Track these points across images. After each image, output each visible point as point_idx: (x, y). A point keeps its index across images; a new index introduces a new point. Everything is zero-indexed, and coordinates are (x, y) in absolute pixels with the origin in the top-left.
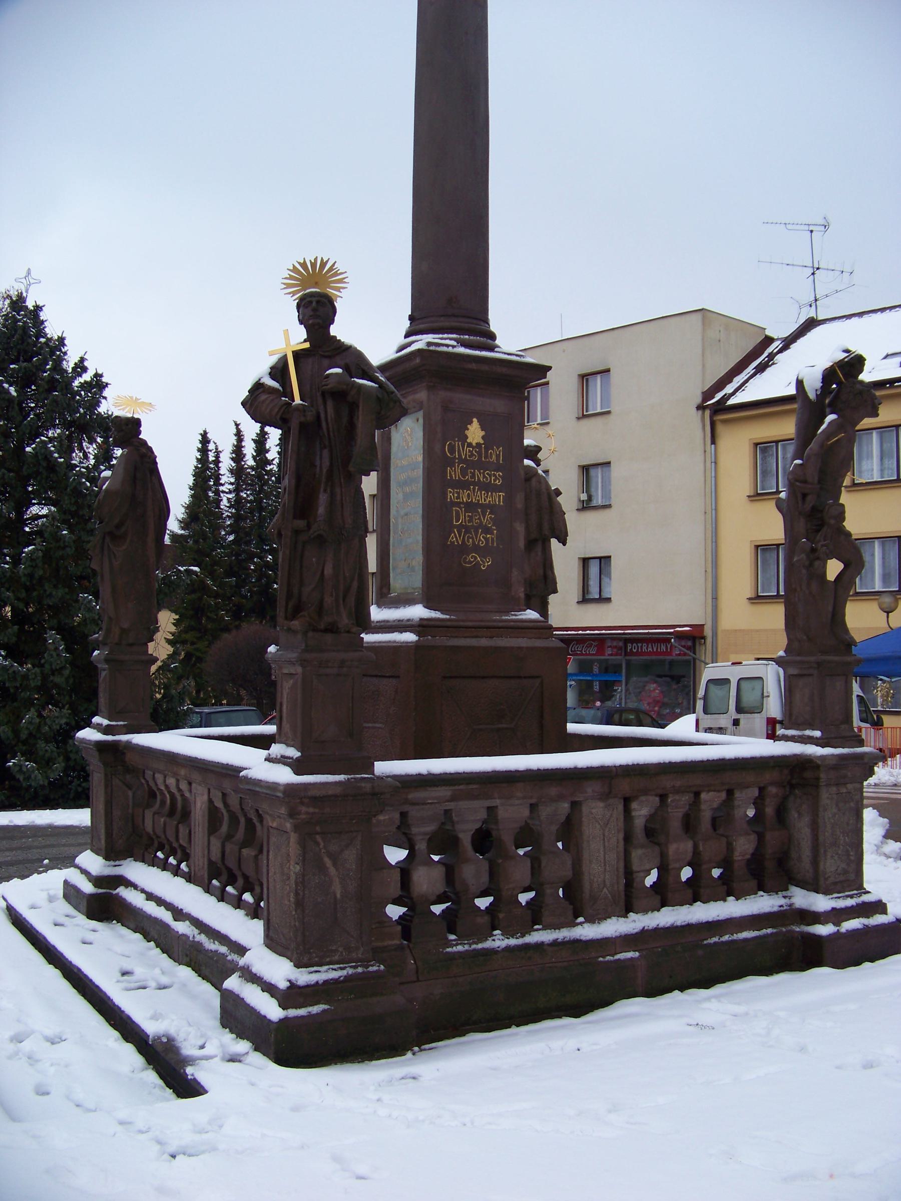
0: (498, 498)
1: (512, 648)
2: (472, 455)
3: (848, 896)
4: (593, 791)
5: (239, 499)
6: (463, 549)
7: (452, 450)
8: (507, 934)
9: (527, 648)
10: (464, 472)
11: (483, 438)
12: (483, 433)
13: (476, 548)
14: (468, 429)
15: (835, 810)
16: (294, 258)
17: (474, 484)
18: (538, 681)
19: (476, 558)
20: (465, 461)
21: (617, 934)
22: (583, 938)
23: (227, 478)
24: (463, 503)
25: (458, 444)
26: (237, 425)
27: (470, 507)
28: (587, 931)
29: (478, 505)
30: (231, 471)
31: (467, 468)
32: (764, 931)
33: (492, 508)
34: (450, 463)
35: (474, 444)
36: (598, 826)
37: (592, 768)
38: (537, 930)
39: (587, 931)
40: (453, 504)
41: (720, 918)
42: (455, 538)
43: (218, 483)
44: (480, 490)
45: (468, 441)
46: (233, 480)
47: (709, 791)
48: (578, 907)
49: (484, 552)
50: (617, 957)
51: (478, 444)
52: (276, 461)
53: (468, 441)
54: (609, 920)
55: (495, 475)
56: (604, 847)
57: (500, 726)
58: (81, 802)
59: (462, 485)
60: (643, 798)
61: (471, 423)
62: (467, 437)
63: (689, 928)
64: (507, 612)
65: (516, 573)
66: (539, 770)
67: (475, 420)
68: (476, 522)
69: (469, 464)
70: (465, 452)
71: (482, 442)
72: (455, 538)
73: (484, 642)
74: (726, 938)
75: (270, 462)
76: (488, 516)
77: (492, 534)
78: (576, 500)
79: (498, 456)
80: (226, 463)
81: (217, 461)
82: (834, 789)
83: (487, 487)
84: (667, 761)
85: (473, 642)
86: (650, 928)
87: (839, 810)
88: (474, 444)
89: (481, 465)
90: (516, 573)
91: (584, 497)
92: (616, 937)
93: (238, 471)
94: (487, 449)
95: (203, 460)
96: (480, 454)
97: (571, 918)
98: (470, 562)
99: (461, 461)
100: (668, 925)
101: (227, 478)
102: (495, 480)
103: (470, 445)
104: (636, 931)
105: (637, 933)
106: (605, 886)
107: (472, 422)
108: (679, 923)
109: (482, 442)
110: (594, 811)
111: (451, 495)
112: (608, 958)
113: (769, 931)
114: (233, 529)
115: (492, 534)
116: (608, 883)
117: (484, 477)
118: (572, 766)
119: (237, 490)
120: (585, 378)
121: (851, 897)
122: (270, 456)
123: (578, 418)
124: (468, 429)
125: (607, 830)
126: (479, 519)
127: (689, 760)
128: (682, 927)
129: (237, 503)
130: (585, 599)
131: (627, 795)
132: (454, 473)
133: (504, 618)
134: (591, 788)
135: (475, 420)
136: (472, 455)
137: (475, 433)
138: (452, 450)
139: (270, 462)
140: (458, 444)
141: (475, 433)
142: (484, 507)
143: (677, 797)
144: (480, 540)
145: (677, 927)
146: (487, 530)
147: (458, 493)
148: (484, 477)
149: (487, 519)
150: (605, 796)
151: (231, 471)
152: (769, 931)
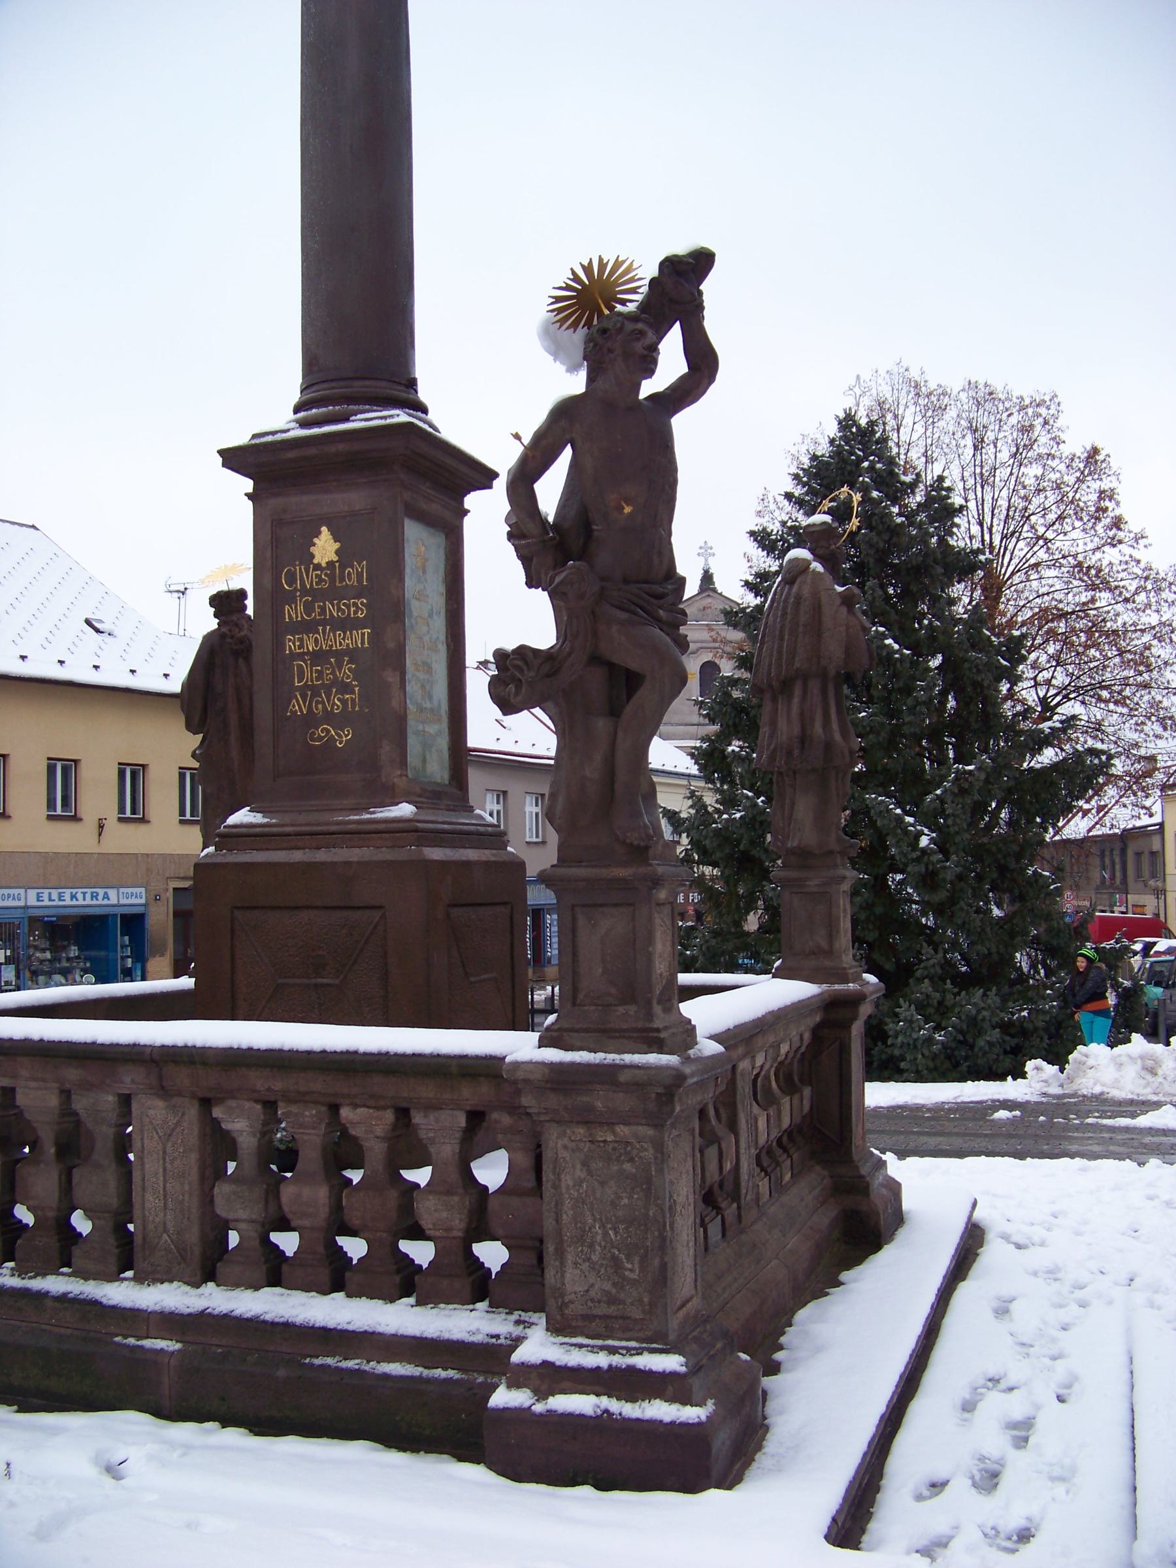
0: (359, 638)
1: (334, 864)
2: (321, 580)
3: (602, 1348)
4: (133, 1081)
6: (311, 720)
7: (291, 580)
8: (20, 1272)
9: (358, 862)
10: (309, 608)
11: (337, 552)
12: (337, 545)
13: (329, 717)
14: (314, 545)
15: (580, 1173)
17: (324, 623)
18: (377, 914)
19: (328, 731)
20: (311, 592)
21: (157, 1308)
22: (104, 1301)
24: (308, 653)
25: (299, 569)
27: (318, 657)
28: (122, 1293)
29: (330, 652)
31: (313, 602)
32: (440, 1373)
33: (352, 654)
34: (290, 599)
35: (324, 565)
36: (156, 1137)
37: (420, 1055)
38: (63, 1274)
39: (122, 1293)
40: (294, 656)
41: (350, 1328)
42: (298, 706)
44: (333, 630)
45: (315, 561)
47: (356, 1106)
48: (126, 1258)
49: (339, 721)
50: (148, 1343)
51: (330, 564)
53: (315, 561)
54: (166, 1285)
55: (355, 604)
56: (165, 1169)
57: (320, 980)
58: (886, 1074)
59: (308, 627)
60: (232, 1103)
61: (318, 534)
62: (313, 556)
63: (286, 1329)
64: (366, 809)
65: (388, 748)
66: (324, 1052)
67: (324, 529)
68: (328, 676)
70: (310, 580)
71: (335, 558)
72: (298, 706)
73: (297, 856)
74: (351, 1364)
76: (346, 669)
77: (353, 692)
79: (360, 575)
82: (581, 1131)
83: (346, 624)
84: (244, 1046)
86: (216, 1312)
87: (590, 1173)
88: (324, 565)
89: (334, 593)
90: (388, 748)
92: (155, 1312)
94: (343, 567)
97: (114, 1268)
98: (320, 738)
99: (305, 592)
100: (249, 1315)
102: (356, 612)
103: (318, 567)
104: (188, 1311)
105: (190, 1315)
106: (165, 1230)
107: (320, 533)
108: (268, 1317)
109: (335, 558)
110: (151, 1112)
111: (291, 644)
112: (132, 1341)
113: (451, 1373)
115: (353, 692)
116: (170, 1226)
117: (339, 609)
118: (89, 1040)
121: (613, 1351)
124: (314, 545)
125: (170, 1144)
126: (333, 673)
127: (180, 1043)
128: (273, 1324)
131: (209, 1095)
132: (293, 612)
133: (352, 817)
134: (129, 1078)
135: (324, 529)
136: (321, 580)
137: (325, 548)
138: (291, 580)
140: (299, 569)
141: (325, 548)
142: (339, 654)
143: (294, 1109)
144: (334, 704)
145: (265, 1322)
146: (345, 688)
147: (301, 640)
148: (339, 609)
149: (346, 672)
150: (163, 1091)
152: (451, 1373)
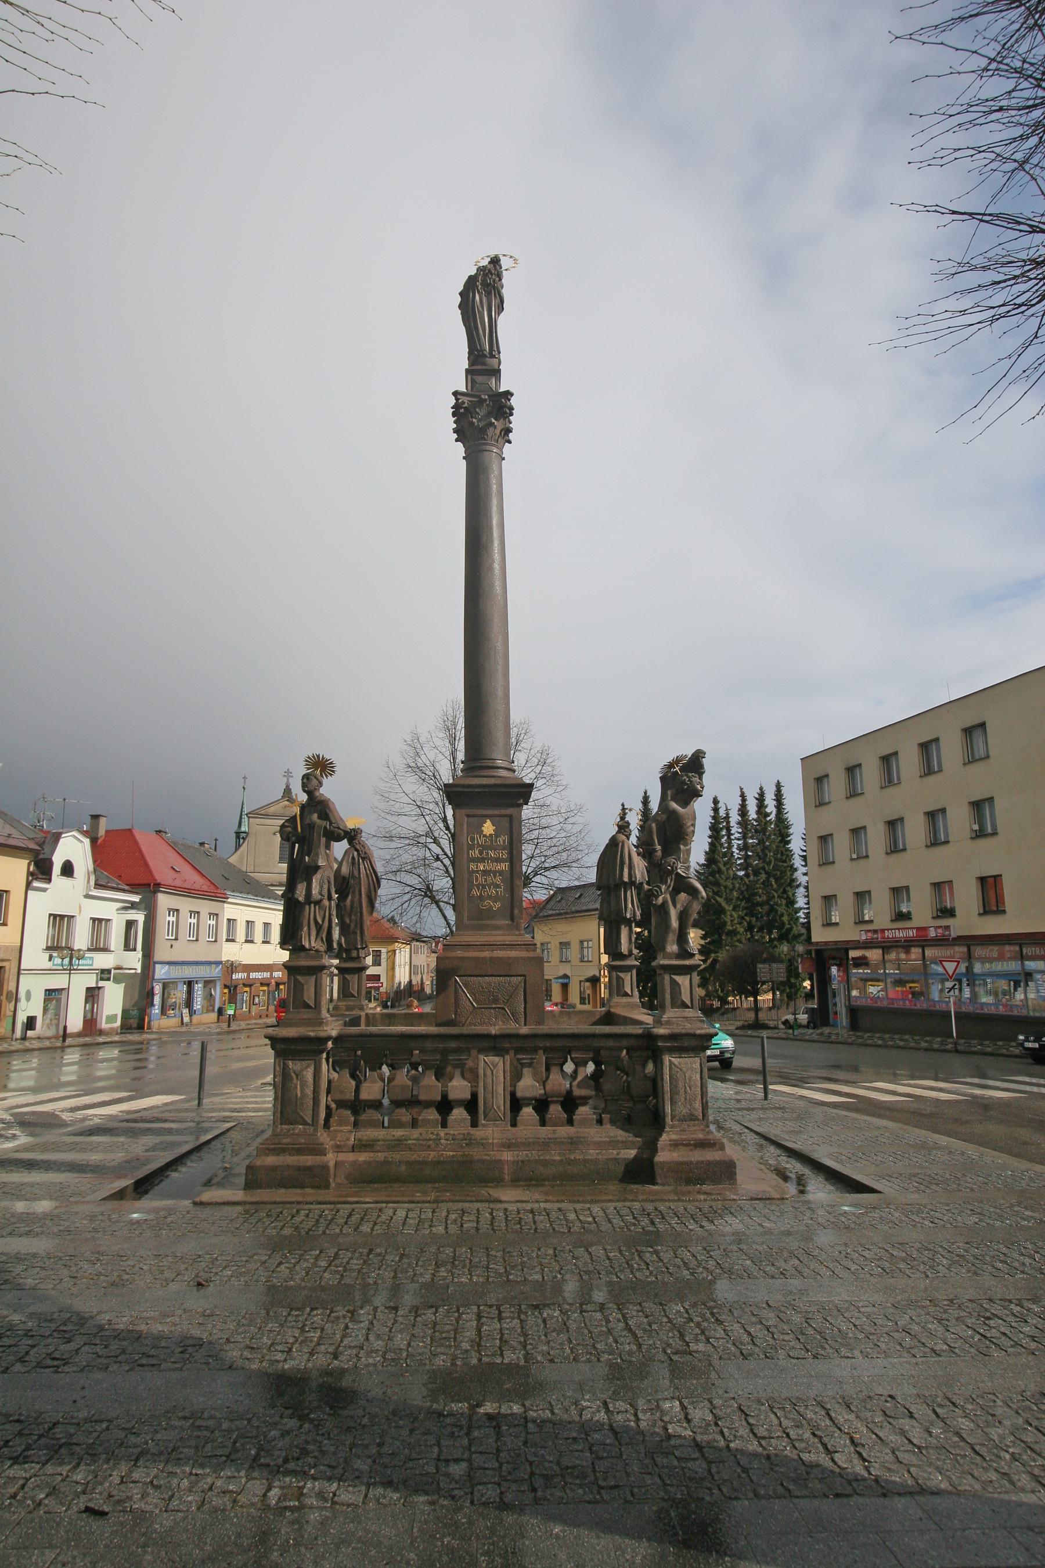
5: (746, 844)
7: (473, 839)
10: (481, 852)
13: (490, 897)
16: (304, 756)
20: (482, 846)
23: (736, 830)
26: (741, 789)
29: (490, 871)
30: (739, 823)
33: (501, 873)
42: (476, 892)
43: (729, 834)
46: (740, 830)
49: (495, 899)
51: (491, 835)
52: (774, 813)
69: (483, 848)
72: (476, 892)
75: (768, 815)
78: (968, 829)
79: (504, 841)
80: (735, 818)
81: (727, 817)
83: (498, 860)
85: (476, 954)
91: (976, 827)
93: (744, 822)
95: (716, 817)
96: (492, 841)
101: (736, 830)
103: (485, 836)
114: (745, 866)
119: (744, 837)
120: (968, 732)
122: (768, 810)
123: (964, 764)
129: (745, 847)
130: (986, 912)
138: (473, 839)
139: (768, 815)
141: (488, 828)
142: (495, 873)
149: (498, 880)
151: (739, 823)
